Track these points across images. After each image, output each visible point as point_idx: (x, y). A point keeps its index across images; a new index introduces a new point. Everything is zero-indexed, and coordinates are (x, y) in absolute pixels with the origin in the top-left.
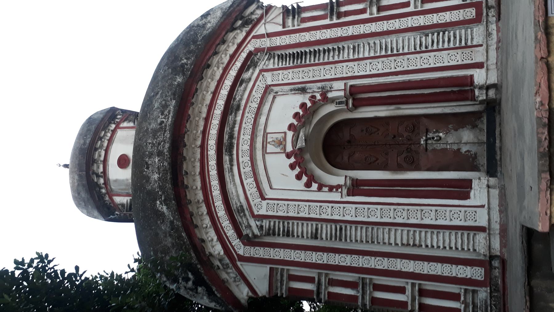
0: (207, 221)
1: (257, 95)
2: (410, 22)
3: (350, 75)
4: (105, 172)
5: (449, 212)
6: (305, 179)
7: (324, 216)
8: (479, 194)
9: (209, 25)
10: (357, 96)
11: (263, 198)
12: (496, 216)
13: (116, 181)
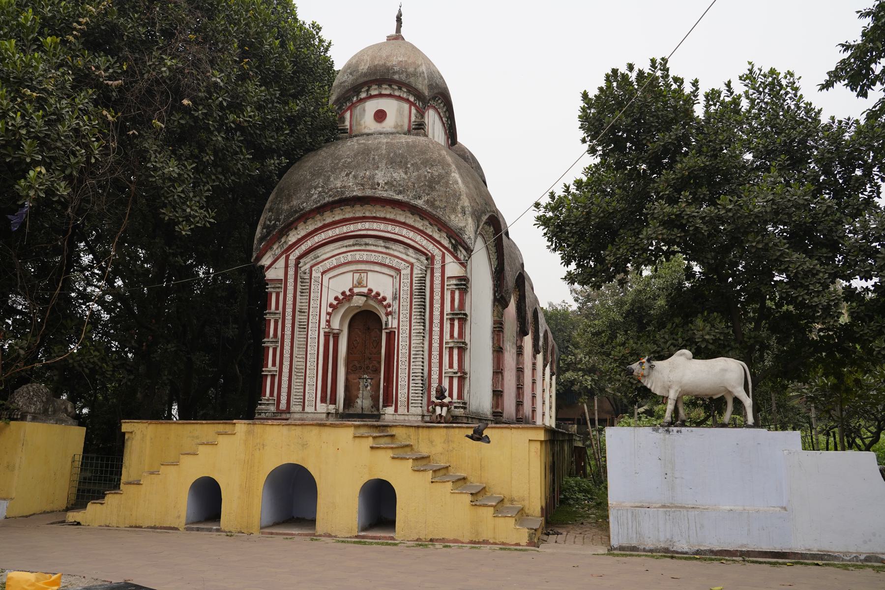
0: (311, 228)
1: (395, 263)
4: (371, 97)
6: (335, 303)
8: (322, 408)
9: (453, 217)
10: (391, 335)
11: (323, 273)
13: (364, 110)
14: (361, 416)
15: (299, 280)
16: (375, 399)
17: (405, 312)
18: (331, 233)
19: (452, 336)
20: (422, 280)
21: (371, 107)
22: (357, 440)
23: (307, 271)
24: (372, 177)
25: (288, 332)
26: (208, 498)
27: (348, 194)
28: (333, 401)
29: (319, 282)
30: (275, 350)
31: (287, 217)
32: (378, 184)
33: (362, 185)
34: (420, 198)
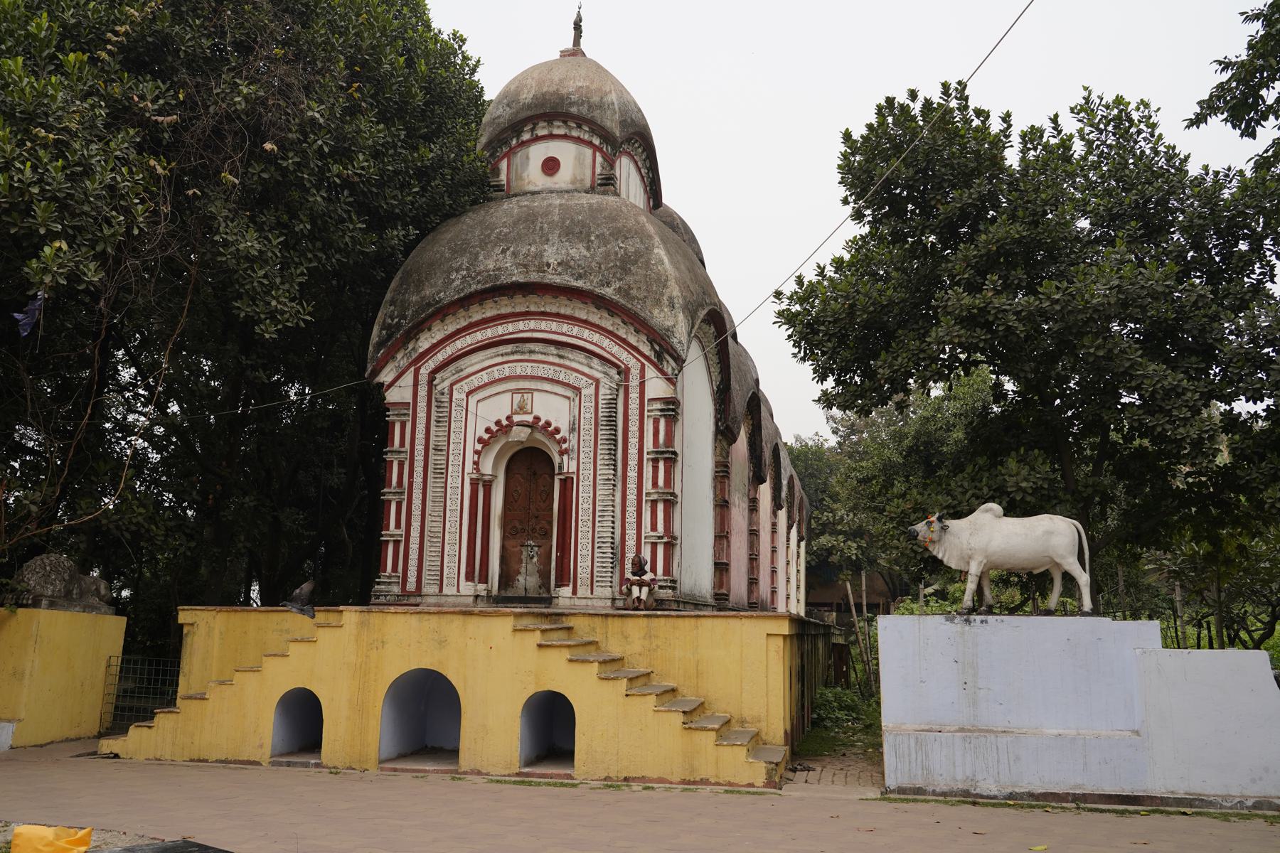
0: (451, 329)
1: (572, 378)
2: (631, 532)
3: (581, 477)
5: (455, 562)
6: (486, 436)
7: (451, 457)
8: (467, 588)
9: (656, 312)
10: (567, 484)
11: (468, 394)
12: (450, 600)
13: (528, 158)
14: (524, 600)
15: (434, 403)
16: (544, 575)
17: (587, 450)
18: (480, 336)
19: (655, 484)
20: (612, 404)
21: (538, 153)
22: (519, 635)
23: (446, 391)
24: (539, 255)
25: (418, 479)
26: (303, 719)
27: (504, 280)
28: (484, 579)
29: (463, 407)
30: (399, 505)
31: (417, 313)
32: (548, 265)
33: (525, 266)
34: (608, 284)
